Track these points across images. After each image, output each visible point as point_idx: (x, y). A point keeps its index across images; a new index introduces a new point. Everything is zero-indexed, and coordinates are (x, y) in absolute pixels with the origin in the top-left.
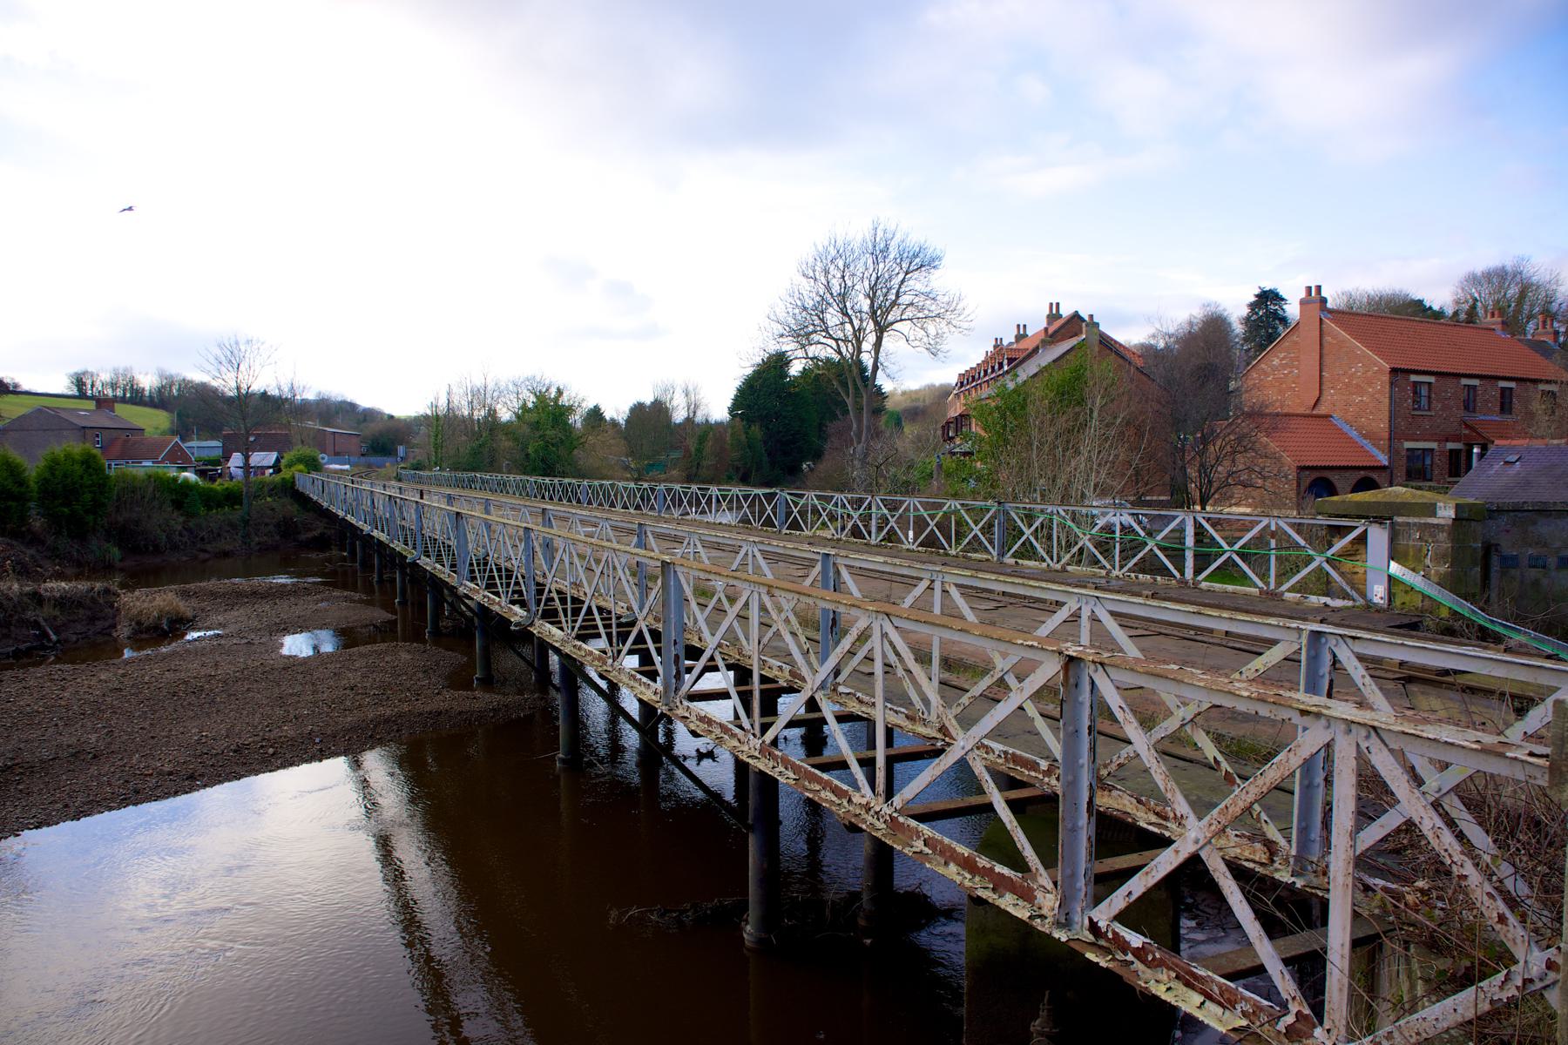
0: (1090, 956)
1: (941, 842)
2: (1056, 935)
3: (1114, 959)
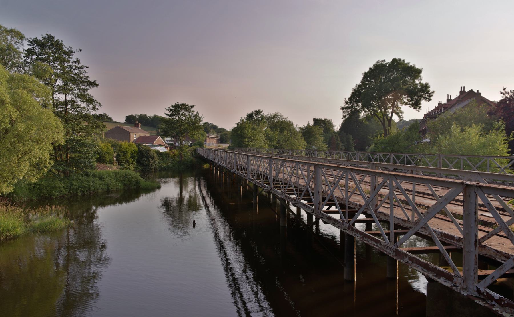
0: (476, 301)
1: (415, 258)
2: (462, 293)
3: (487, 303)
